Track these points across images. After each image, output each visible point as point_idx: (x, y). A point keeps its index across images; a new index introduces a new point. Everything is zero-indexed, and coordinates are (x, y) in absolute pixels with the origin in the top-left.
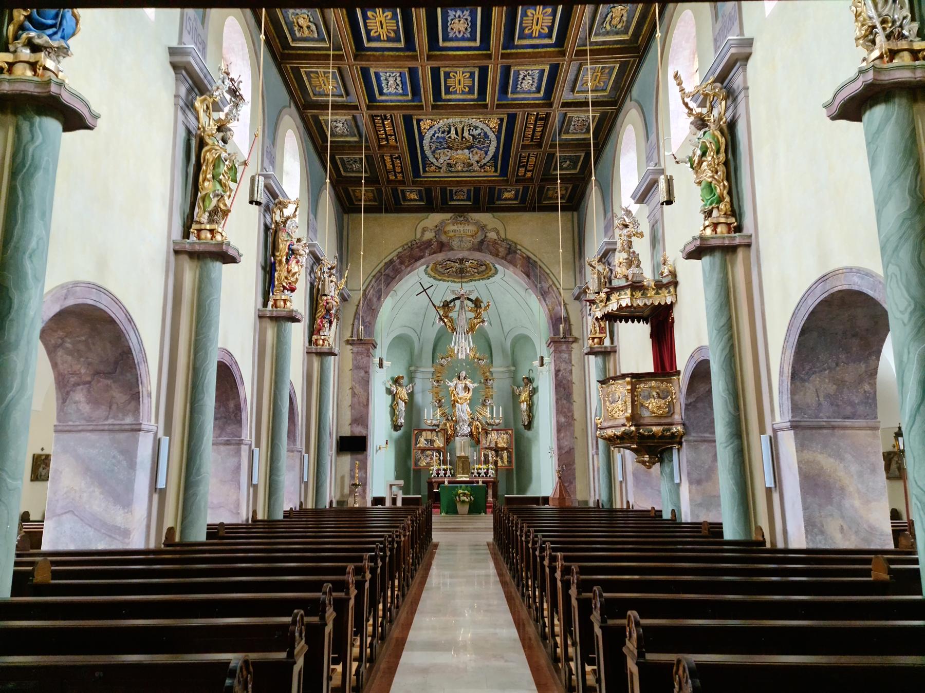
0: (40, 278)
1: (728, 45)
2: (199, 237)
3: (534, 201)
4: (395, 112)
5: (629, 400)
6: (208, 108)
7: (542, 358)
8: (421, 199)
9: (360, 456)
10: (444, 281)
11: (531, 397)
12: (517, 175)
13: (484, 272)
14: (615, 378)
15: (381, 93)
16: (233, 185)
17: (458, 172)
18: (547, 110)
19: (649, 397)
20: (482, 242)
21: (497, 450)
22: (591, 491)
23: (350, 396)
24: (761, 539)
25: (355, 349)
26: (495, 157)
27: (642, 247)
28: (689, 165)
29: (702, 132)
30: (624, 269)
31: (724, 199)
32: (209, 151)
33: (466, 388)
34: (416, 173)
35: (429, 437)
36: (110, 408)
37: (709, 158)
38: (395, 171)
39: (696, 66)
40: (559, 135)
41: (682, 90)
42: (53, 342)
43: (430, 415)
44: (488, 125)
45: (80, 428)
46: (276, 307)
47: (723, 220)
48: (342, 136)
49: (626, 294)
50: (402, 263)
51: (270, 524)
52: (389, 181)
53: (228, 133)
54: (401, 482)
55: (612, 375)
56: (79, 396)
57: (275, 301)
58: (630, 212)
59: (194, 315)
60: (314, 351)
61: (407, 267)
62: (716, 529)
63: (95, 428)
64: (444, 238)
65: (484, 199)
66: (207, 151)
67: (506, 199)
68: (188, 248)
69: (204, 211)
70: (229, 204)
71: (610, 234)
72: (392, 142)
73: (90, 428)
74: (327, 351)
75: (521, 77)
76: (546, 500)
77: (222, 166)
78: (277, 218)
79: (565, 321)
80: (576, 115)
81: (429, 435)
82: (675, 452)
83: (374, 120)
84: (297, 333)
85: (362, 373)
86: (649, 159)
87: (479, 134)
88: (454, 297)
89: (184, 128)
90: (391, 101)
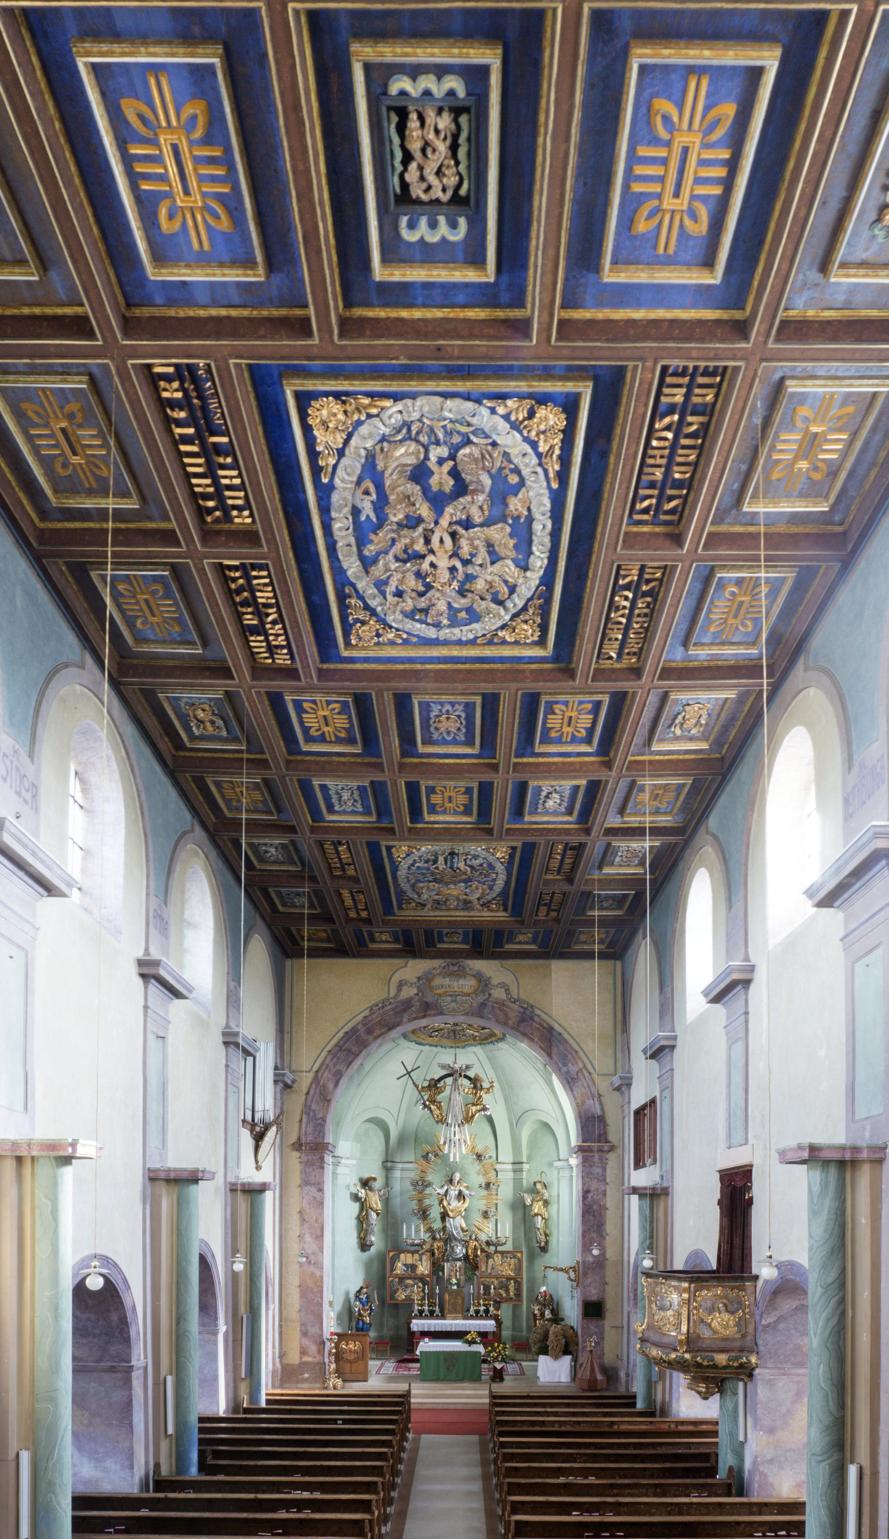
1: (870, 834)
3: (556, 945)
8: (396, 941)
18: (583, 839)
20: (483, 1005)
26: (504, 893)
48: (275, 862)
50: (369, 1032)
52: (348, 919)
61: (376, 1038)
64: (429, 999)
65: (484, 943)
72: (351, 871)
75: (544, 794)
79: (600, 1121)
80: (623, 845)
87: (481, 865)
88: (444, 1072)
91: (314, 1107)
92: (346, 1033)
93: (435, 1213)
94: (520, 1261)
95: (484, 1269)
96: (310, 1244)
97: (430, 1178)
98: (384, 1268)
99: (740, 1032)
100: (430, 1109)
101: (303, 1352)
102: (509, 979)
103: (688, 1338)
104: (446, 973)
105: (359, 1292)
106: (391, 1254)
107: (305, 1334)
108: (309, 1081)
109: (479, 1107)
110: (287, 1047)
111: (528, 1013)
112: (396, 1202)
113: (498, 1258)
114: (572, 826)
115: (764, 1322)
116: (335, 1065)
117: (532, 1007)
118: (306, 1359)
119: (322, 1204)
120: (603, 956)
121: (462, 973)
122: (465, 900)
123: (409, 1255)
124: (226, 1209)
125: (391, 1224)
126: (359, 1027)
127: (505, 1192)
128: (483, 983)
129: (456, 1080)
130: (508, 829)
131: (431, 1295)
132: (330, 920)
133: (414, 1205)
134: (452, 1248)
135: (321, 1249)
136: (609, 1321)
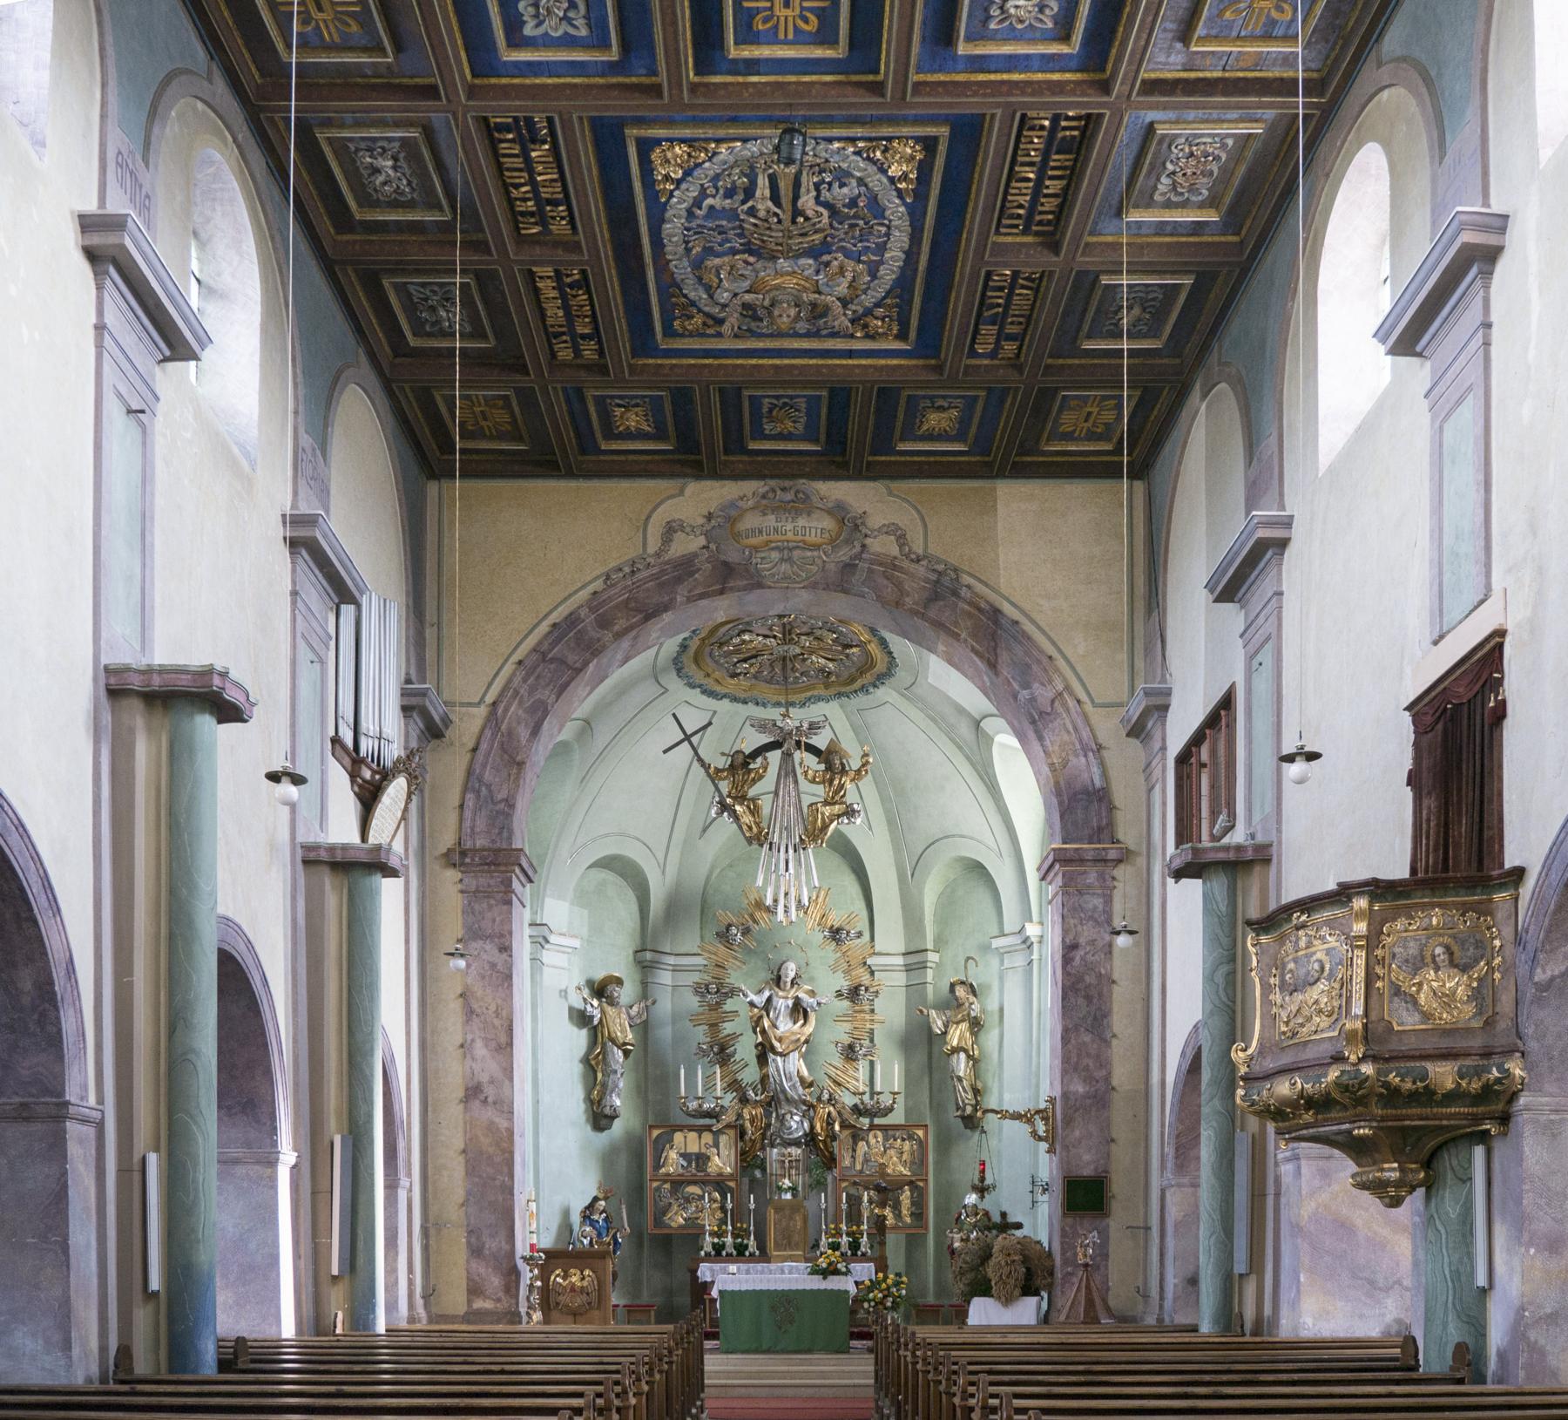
3: (1011, 444)
8: (660, 435)
13: (860, 673)
15: (516, 38)
20: (849, 567)
22: (1170, 1262)
25: (471, 883)
26: (903, 284)
34: (643, 341)
35: (693, 1148)
39: (1386, 270)
48: (395, 204)
50: (604, 623)
61: (619, 636)
64: (733, 556)
65: (856, 432)
81: (690, 1142)
83: (493, 144)
87: (853, 203)
88: (766, 739)
91: (488, 776)
92: (554, 625)
93: (745, 1050)
94: (922, 1145)
95: (847, 1162)
96: (485, 1064)
97: (734, 978)
98: (640, 1167)
99: (1467, 397)
101: (474, 1290)
102: (903, 516)
103: (1365, 1026)
104: (766, 505)
105: (591, 1207)
106: (656, 1133)
107: (476, 1252)
108: (478, 723)
109: (837, 809)
111: (946, 581)
112: (665, 1033)
113: (875, 1139)
115: (1540, 976)
116: (532, 690)
117: (956, 570)
118: (479, 1304)
119: (510, 977)
121: (802, 505)
122: (814, 305)
123: (693, 1135)
124: (294, 898)
125: (654, 1080)
126: (583, 613)
127: (890, 1010)
128: (850, 525)
129: (788, 756)
130: (917, 85)
131: (739, 1214)
133: (700, 1034)
134: (781, 1119)
135: (509, 1072)
136: (1117, 1220)
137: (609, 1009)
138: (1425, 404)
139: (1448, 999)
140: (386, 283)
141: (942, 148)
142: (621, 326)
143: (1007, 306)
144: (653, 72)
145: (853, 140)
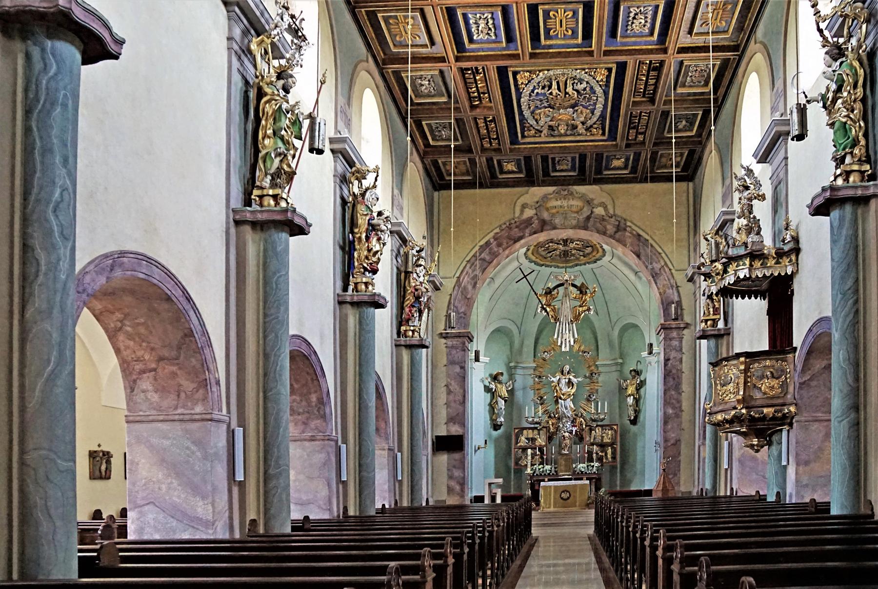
0: (69, 235)
2: (261, 205)
3: (646, 172)
4: (487, 63)
5: (742, 381)
6: (266, 52)
7: (651, 345)
8: (520, 172)
9: (457, 456)
10: (547, 266)
11: (638, 390)
12: (628, 139)
14: (727, 359)
15: (471, 41)
16: (298, 143)
17: (561, 135)
18: (660, 57)
19: (762, 377)
20: (588, 218)
21: (603, 446)
22: (695, 481)
23: (445, 393)
24: (870, 513)
26: (603, 117)
27: (762, 210)
28: (821, 104)
29: (838, 63)
30: (744, 236)
31: (859, 142)
32: (269, 101)
33: (570, 383)
34: (514, 140)
35: (531, 436)
36: (178, 396)
37: (845, 94)
38: (490, 138)
40: (675, 89)
41: (817, 13)
42: (112, 325)
43: (531, 412)
44: (594, 78)
45: (151, 418)
46: (357, 291)
47: (856, 167)
49: (744, 264)
50: (499, 245)
51: (363, 521)
52: (483, 149)
53: (290, 80)
54: (500, 480)
55: (724, 355)
56: (146, 384)
57: (356, 284)
58: (752, 171)
59: (260, 291)
60: (403, 343)
62: (825, 508)
63: (166, 418)
64: (546, 215)
65: (590, 169)
66: (266, 103)
67: (615, 169)
68: (249, 217)
69: (266, 174)
70: (293, 165)
71: (728, 203)
73: (161, 418)
74: (417, 343)
75: (632, 15)
76: (649, 493)
77: (283, 118)
78: (356, 190)
82: (784, 433)
84: (383, 321)
85: (457, 369)
86: (774, 109)
87: (585, 89)
89: (240, 77)
90: (483, 50)
95: (588, 439)
100: (546, 311)
104: (558, 195)
107: (450, 477)
109: (584, 308)
110: (435, 237)
114: (653, 47)
117: (625, 220)
120: (679, 179)
122: (573, 125)
126: (492, 240)
132: (470, 150)
137: (498, 385)
138: (770, 182)
139: (772, 388)
140: (424, 123)
141: (614, 71)
142: (507, 135)
143: (639, 123)
144: (517, 49)
145: (584, 69)
